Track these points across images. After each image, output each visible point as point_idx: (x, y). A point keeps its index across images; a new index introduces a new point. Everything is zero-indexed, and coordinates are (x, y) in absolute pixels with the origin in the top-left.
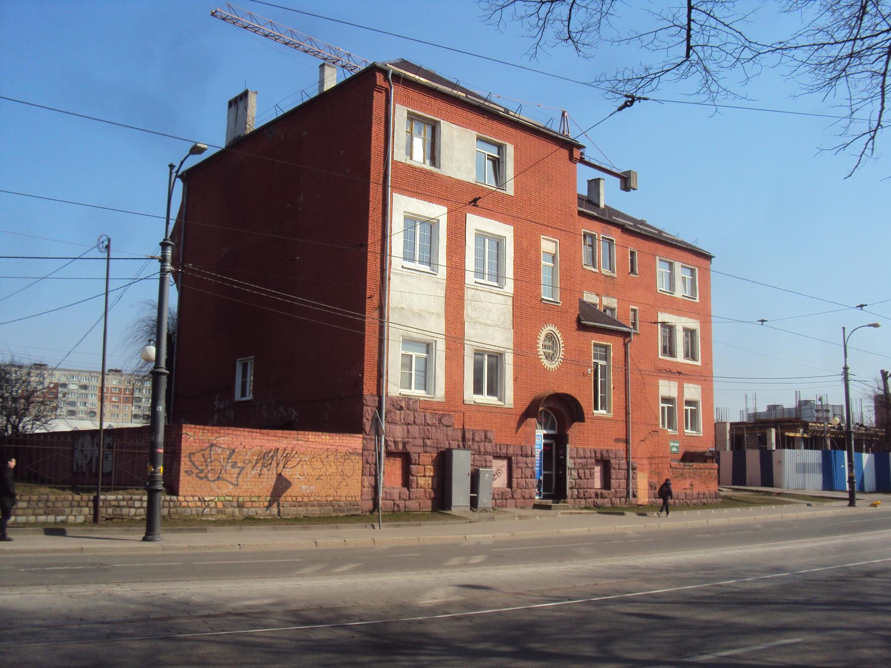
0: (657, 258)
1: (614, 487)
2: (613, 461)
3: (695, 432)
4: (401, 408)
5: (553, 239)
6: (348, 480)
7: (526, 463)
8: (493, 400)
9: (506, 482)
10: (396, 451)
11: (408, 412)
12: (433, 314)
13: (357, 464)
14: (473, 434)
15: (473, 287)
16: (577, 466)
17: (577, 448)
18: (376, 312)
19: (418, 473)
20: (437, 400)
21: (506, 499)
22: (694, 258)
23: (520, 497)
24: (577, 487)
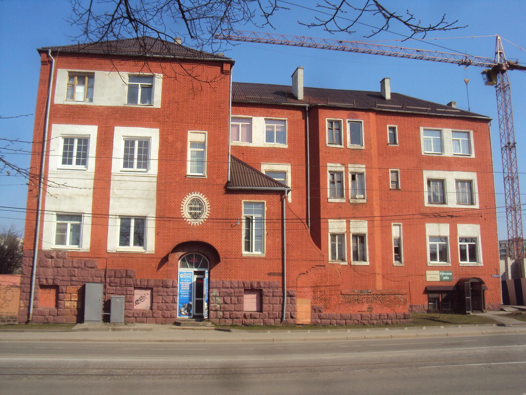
0: (422, 129)
1: (267, 310)
2: (264, 290)
3: (445, 263)
4: (52, 258)
5: (202, 132)
6: (8, 302)
7: (167, 292)
8: (139, 249)
9: (149, 305)
10: (47, 284)
11: (58, 259)
12: (83, 195)
13: (17, 293)
14: (115, 273)
15: (119, 174)
16: (222, 294)
17: (223, 281)
18: (35, 199)
19: (64, 298)
20: (83, 251)
21: (146, 317)
22: (470, 123)
23: (161, 316)
24: (222, 310)
